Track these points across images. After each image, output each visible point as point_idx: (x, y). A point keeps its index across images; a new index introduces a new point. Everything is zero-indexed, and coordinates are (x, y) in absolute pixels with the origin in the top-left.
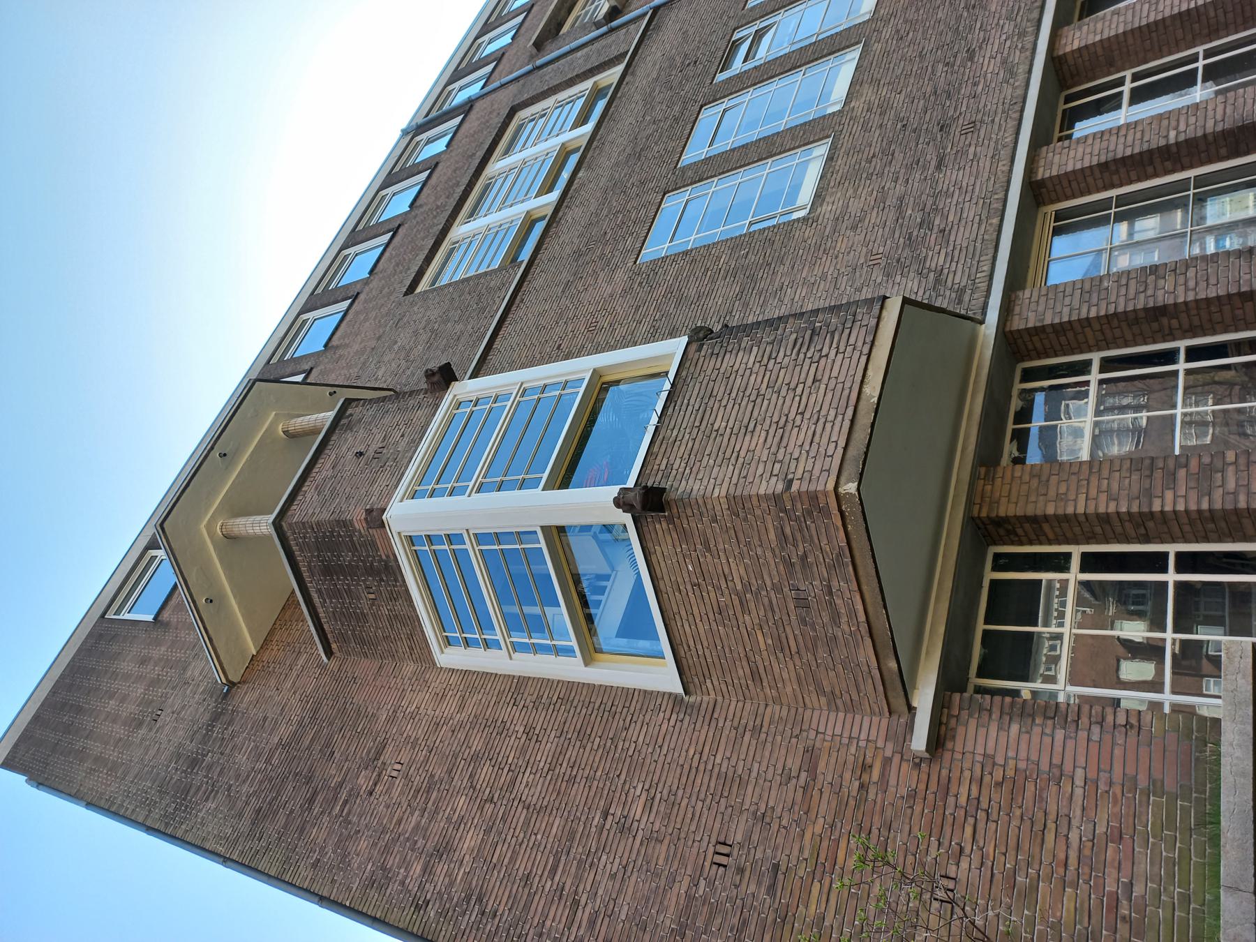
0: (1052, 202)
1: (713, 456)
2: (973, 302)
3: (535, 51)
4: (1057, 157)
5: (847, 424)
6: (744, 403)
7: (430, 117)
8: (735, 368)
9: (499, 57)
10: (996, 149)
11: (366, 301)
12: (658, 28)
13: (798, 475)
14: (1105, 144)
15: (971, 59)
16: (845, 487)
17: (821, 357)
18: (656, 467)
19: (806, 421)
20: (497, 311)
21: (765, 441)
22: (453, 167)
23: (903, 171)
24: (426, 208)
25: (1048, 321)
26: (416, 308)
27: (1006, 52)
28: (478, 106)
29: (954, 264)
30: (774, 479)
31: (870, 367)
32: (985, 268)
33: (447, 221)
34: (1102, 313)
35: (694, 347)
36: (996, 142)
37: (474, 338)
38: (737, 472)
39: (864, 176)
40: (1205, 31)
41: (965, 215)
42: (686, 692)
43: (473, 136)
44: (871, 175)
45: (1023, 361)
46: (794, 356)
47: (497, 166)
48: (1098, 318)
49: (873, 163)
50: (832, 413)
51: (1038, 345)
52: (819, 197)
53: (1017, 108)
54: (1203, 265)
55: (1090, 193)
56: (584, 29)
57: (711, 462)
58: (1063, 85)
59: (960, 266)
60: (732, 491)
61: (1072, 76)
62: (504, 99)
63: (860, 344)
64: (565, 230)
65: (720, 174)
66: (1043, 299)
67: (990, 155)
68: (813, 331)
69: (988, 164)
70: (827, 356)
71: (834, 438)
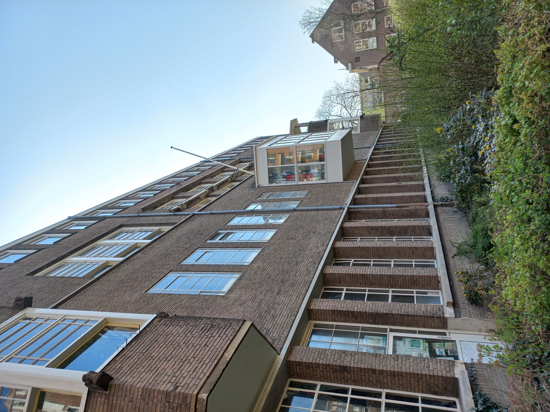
0: (314, 320)
1: (145, 368)
2: (278, 345)
3: (141, 211)
4: (318, 303)
5: (213, 366)
6: (170, 347)
8: (172, 332)
9: (125, 209)
10: (299, 294)
11: (4, 272)
12: (193, 220)
13: (182, 385)
14: (334, 304)
15: (297, 265)
16: (202, 395)
17: (211, 336)
18: (114, 367)
19: (195, 361)
20: (69, 294)
21: (173, 366)
22: (83, 236)
23: (265, 291)
24: (61, 246)
25: (304, 361)
26: (28, 282)
27: (308, 266)
28: (107, 220)
29: (274, 329)
30: (170, 384)
31: (230, 345)
32: (285, 334)
33: (68, 253)
34: (324, 363)
35: (158, 319)
36: (299, 292)
37: (50, 302)
38: (153, 377)
39: (250, 288)
40: (369, 283)
41: (283, 313)
43: (99, 228)
44: (252, 289)
45: (291, 377)
46: (200, 333)
47: (105, 241)
48: (322, 364)
49: (255, 285)
50: (208, 360)
51: (298, 371)
52: (231, 290)
53: (309, 284)
54: (360, 355)
55: (327, 321)
56: (164, 211)
57: (143, 370)
58: (325, 284)
59: (276, 330)
60: (147, 386)
61: (328, 282)
62: (120, 221)
63: (229, 335)
64: (121, 272)
65: (196, 271)
66: (304, 351)
67: (296, 295)
68: (212, 325)
69: (295, 298)
70: (214, 337)
71: (205, 372)
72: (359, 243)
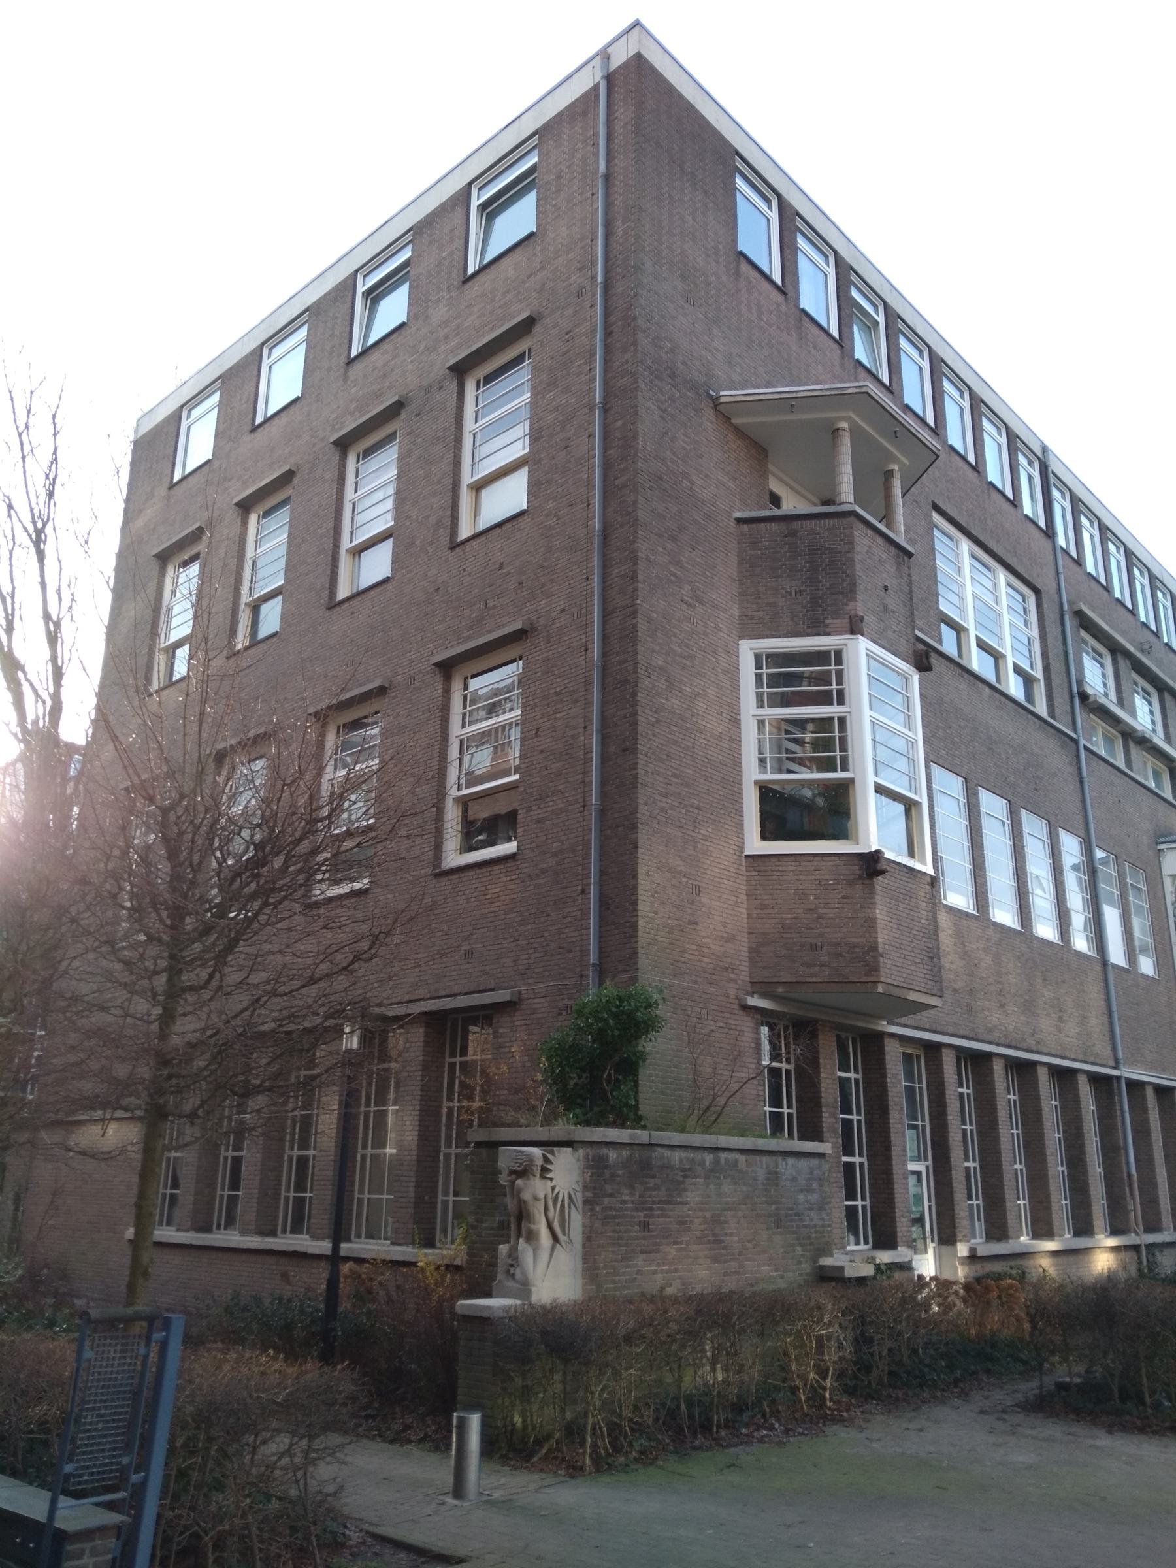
7: (1051, 475)
42: (747, 856)
47: (1002, 576)
72: (1050, 1103)
